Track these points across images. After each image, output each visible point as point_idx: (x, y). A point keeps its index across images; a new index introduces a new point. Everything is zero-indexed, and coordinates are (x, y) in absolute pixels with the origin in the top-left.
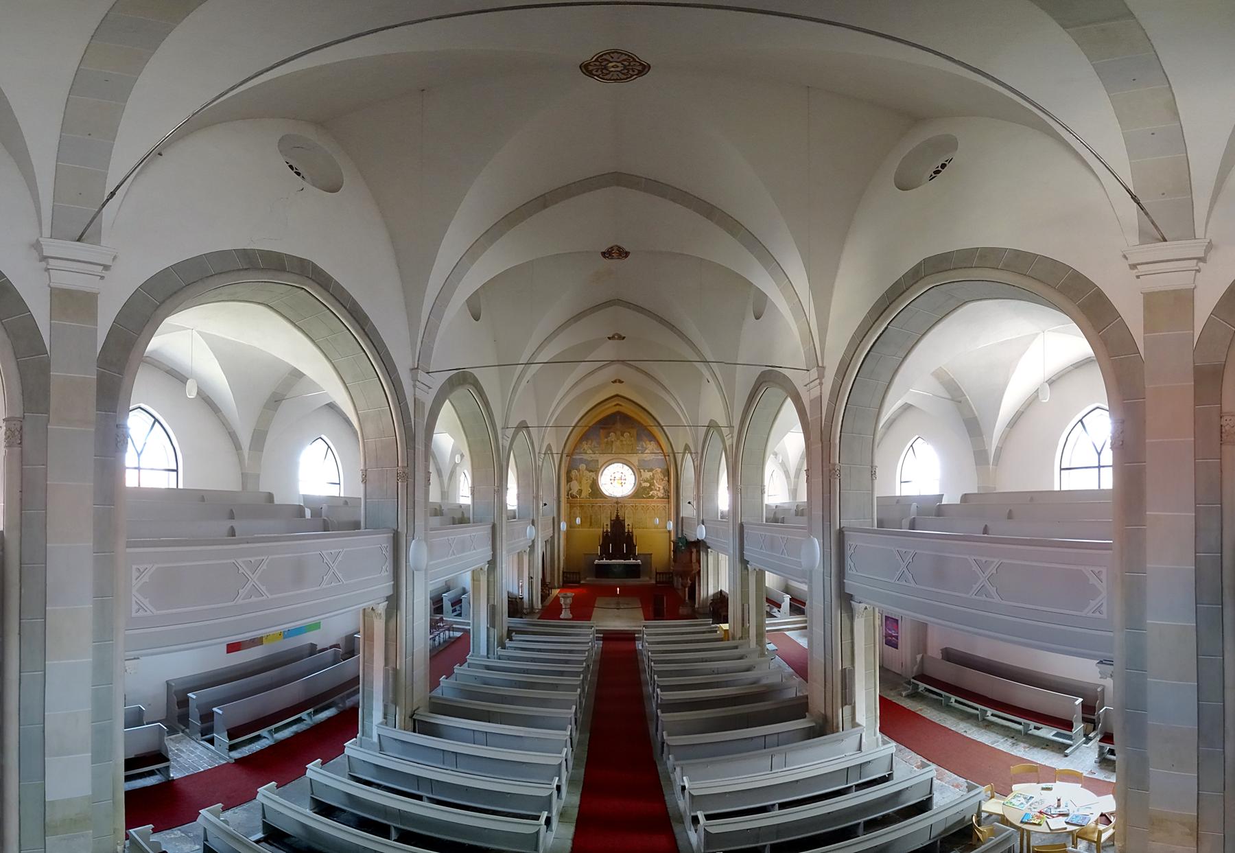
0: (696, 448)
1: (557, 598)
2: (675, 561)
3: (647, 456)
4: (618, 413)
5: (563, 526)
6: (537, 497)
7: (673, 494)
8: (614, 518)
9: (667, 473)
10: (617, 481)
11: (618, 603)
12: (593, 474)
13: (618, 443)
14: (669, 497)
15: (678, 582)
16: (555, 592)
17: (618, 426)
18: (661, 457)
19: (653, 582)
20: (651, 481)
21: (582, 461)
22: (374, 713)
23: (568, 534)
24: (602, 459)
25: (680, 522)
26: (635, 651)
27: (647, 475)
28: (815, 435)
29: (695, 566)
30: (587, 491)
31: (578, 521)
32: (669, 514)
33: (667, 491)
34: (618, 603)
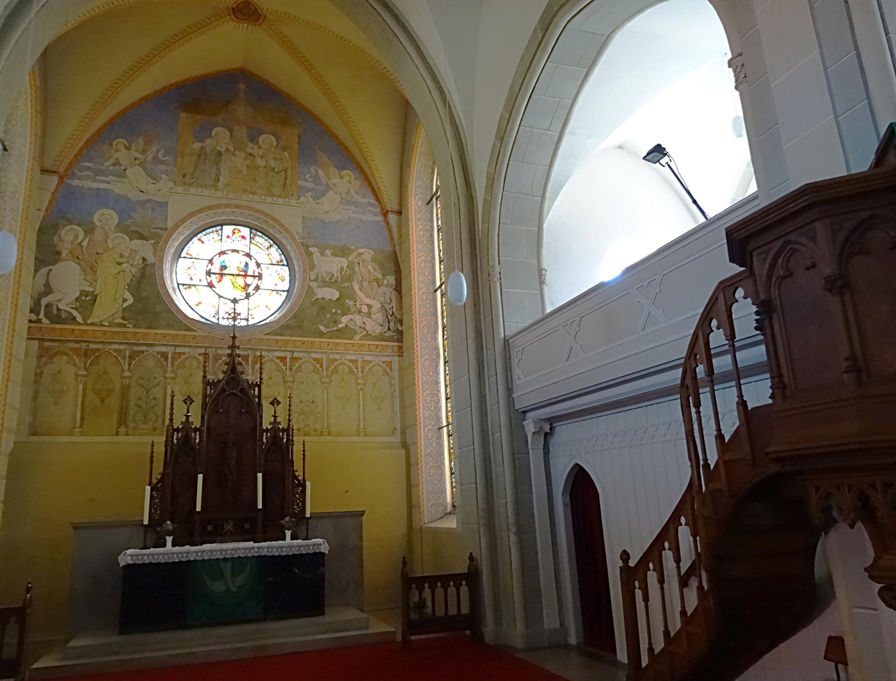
8: (217, 373)
12: (144, 249)
13: (239, 160)
17: (241, 110)
18: (372, 216)
20: (342, 283)
21: (103, 199)
22: (837, 590)
24: (182, 202)
27: (332, 265)
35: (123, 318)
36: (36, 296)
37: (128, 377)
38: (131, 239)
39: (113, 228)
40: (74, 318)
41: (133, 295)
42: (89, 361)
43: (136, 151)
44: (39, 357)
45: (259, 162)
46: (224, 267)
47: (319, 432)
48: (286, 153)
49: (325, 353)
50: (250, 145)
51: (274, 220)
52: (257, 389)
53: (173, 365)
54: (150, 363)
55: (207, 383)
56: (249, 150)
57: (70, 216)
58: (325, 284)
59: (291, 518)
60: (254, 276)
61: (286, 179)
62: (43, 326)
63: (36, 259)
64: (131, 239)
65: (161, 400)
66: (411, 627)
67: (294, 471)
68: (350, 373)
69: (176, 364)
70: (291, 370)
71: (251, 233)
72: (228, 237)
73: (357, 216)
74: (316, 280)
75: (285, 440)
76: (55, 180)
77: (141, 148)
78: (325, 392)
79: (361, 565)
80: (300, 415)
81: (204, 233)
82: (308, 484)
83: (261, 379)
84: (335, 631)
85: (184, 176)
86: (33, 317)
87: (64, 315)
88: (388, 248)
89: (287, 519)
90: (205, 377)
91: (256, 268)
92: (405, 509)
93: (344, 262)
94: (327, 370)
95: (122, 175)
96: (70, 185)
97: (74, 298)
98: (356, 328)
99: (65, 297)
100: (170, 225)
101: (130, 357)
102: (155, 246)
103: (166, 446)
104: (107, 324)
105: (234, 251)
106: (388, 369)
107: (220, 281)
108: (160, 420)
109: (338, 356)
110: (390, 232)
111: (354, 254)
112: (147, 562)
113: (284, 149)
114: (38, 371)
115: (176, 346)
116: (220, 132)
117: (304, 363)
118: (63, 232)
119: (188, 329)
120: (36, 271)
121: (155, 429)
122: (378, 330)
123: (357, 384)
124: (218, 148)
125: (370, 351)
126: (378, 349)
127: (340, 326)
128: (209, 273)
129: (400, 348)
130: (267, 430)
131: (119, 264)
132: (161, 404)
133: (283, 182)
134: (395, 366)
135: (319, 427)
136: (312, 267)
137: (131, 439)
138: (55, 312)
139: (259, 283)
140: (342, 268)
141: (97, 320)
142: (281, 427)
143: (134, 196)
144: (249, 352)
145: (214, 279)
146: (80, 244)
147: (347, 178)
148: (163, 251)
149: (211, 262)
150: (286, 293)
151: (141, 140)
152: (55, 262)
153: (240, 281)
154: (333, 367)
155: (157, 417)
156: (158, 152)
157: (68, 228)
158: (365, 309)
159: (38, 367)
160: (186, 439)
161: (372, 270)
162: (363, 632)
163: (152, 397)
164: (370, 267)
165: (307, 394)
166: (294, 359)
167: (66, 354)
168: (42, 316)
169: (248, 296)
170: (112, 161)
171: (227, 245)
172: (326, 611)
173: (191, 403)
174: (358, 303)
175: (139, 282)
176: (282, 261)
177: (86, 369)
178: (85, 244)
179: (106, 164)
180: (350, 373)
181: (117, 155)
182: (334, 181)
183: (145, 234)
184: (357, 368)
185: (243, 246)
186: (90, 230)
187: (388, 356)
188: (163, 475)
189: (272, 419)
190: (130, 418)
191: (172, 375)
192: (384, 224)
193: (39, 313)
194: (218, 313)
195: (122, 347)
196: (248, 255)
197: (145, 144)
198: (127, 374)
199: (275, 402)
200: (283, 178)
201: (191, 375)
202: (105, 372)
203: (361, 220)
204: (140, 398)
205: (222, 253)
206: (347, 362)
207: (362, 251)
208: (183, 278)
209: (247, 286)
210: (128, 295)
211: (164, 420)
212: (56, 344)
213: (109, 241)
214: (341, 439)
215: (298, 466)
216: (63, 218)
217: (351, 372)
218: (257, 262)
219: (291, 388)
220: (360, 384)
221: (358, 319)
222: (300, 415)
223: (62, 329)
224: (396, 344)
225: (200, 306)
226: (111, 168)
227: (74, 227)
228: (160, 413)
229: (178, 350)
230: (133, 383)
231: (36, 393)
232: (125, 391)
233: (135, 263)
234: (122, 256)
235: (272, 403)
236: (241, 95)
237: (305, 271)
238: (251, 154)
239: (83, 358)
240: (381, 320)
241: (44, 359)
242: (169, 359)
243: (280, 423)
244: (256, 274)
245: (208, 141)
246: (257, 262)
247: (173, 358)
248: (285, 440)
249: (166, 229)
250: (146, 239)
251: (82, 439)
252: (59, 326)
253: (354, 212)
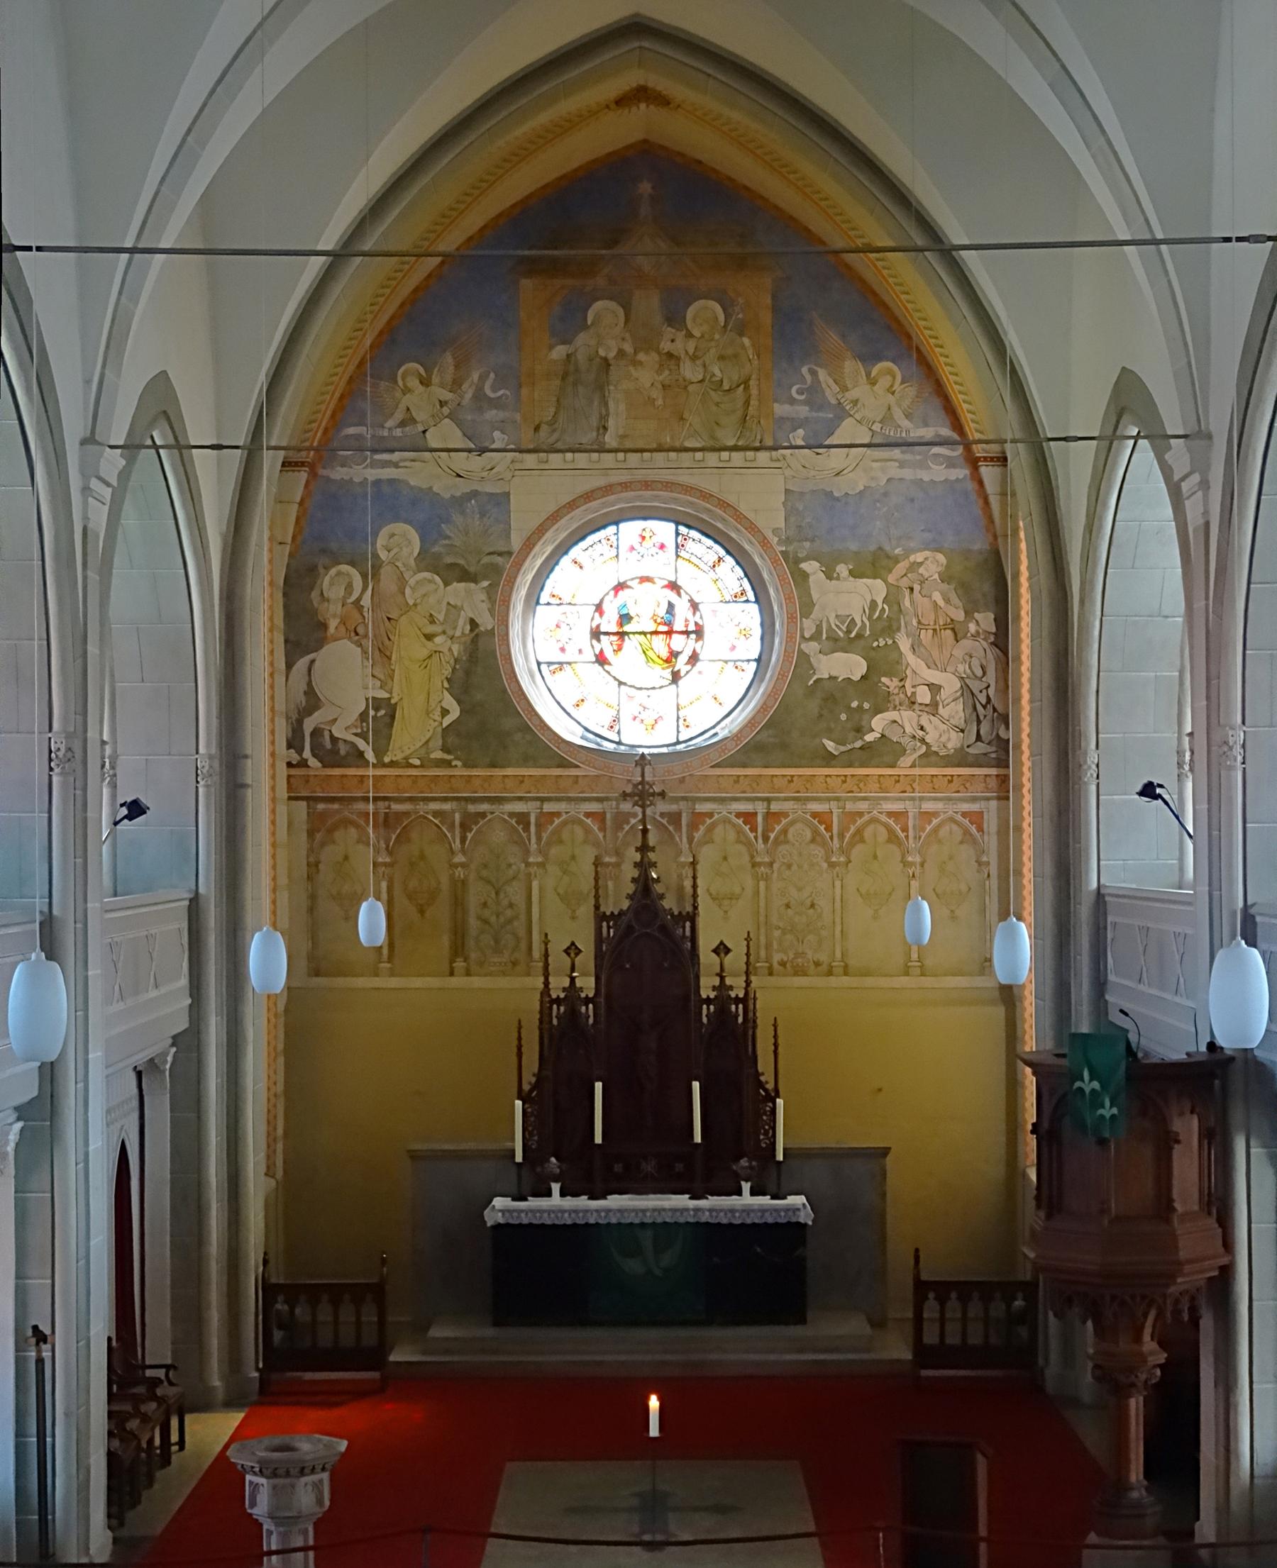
0: (1195, 390)
1: (224, 1478)
2: (1051, 1196)
3: (850, 470)
4: (646, 157)
5: (268, 961)
6: (72, 759)
7: (1034, 727)
8: (618, 899)
9: (991, 584)
10: (637, 639)
11: (653, 1506)
12: (470, 600)
13: (646, 376)
14: (1001, 754)
15: (1070, 1354)
16: (211, 1431)
17: (646, 250)
18: (943, 470)
19: (898, 1350)
20: (874, 638)
21: (392, 502)
23: (300, 1019)
24: (534, 487)
25: (1080, 926)
26: (497, 1227)
27: (848, 598)
28: (1047, 1110)
29: (1192, 1240)
30: (427, 711)
31: (371, 922)
32: (1007, 873)
33: (989, 715)
34: (653, 1506)
35: (445, 749)
36: (295, 716)
37: (463, 865)
38: (446, 584)
39: (412, 562)
40: (361, 754)
41: (459, 702)
42: (394, 837)
43: (442, 386)
44: (311, 833)
45: (690, 371)
46: (625, 618)
47: (825, 967)
48: (746, 341)
49: (837, 799)
50: (669, 332)
51: (724, 505)
52: (688, 924)
53: (539, 838)
54: (498, 836)
55: (600, 917)
56: (666, 346)
57: (334, 546)
58: (837, 644)
59: (750, 1161)
60: (687, 633)
61: (747, 403)
62: (312, 773)
63: (286, 641)
64: (446, 584)
65: (523, 906)
66: (924, 1355)
67: (758, 1074)
68: (889, 841)
69: (545, 836)
70: (766, 839)
71: (677, 534)
72: (632, 548)
73: (907, 474)
74: (816, 637)
75: (740, 1020)
76: (303, 476)
77: (449, 378)
78: (838, 883)
79: (883, 1239)
80: (784, 932)
81: (583, 545)
82: (780, 1102)
83: (695, 908)
84: (815, 1351)
85: (537, 429)
86: (295, 758)
87: (343, 750)
88: (980, 544)
89: (744, 1162)
90: (597, 907)
91: (689, 615)
92: (1002, 1126)
93: (877, 589)
94: (841, 836)
95: (419, 447)
96: (328, 479)
97: (356, 715)
98: (905, 741)
99: (342, 715)
100: (516, 543)
101: (462, 825)
102: (491, 591)
103: (540, 1029)
104: (417, 762)
105: (645, 579)
106: (973, 829)
107: (620, 648)
108: (523, 945)
109: (863, 806)
110: (986, 501)
111: (901, 567)
112: (525, 1221)
113: (741, 330)
114: (311, 859)
115: (542, 800)
116: (604, 310)
117: (792, 823)
118: (327, 580)
119: (564, 764)
120: (289, 666)
121: (514, 964)
122: (954, 741)
123: (906, 864)
124: (602, 353)
125: (934, 790)
126: (955, 786)
127: (869, 738)
128: (596, 634)
129: (1003, 780)
130: (708, 1001)
131: (429, 637)
132: (523, 917)
133: (739, 413)
134: (991, 823)
135: (823, 957)
136: (807, 606)
137: (476, 982)
138: (328, 745)
139: (698, 646)
140: (873, 604)
141: (399, 757)
142: (733, 994)
143: (445, 487)
144: (683, 805)
145: (606, 644)
146: (357, 603)
147: (884, 382)
148: (506, 603)
149: (599, 608)
150: (754, 665)
151: (448, 359)
152: (319, 644)
153: (659, 644)
154: (853, 829)
155: (518, 939)
156: (483, 378)
157: (333, 571)
158: (924, 696)
159: (311, 850)
160: (573, 1014)
161: (941, 603)
162: (865, 1356)
163: (505, 902)
164: (937, 596)
165: (800, 889)
166: (771, 816)
167: (353, 823)
168: (307, 753)
169: (676, 677)
170: (399, 415)
171: (628, 569)
172: (810, 1315)
173: (577, 954)
174: (908, 684)
175: (468, 673)
176: (743, 593)
177: (390, 852)
178: (366, 601)
179: (389, 424)
180: (889, 841)
181: (406, 400)
182: (853, 394)
183: (472, 569)
184: (905, 830)
185: (662, 566)
186: (372, 572)
187: (974, 800)
188: (539, 1076)
189: (717, 981)
190: (471, 943)
191: (540, 859)
192: (971, 486)
193: (303, 750)
194: (616, 720)
195: (447, 807)
196: (674, 586)
197: (457, 367)
198: (459, 858)
199: (722, 949)
200: (740, 404)
201: (573, 857)
202: (422, 857)
203: (919, 483)
204: (485, 905)
205: (620, 587)
206: (884, 818)
207: (919, 557)
208: (547, 652)
209: (674, 655)
210: (450, 702)
211: (530, 949)
212: (336, 806)
213: (408, 591)
214: (869, 981)
215: (764, 1064)
216: (323, 551)
217: (892, 838)
218: (691, 601)
219: (767, 879)
220: (911, 864)
221: (908, 719)
222: (784, 932)
223: (343, 776)
224: (993, 771)
225: (583, 707)
226: (398, 432)
227: (345, 568)
228: (522, 933)
229: (548, 807)
230: (472, 877)
231: (313, 897)
232: (459, 887)
233: (458, 633)
234: (432, 620)
235: (716, 951)
236: (645, 210)
237: (791, 618)
238: (670, 355)
239: (382, 830)
240: (959, 718)
241: (318, 836)
242: (533, 829)
243: (731, 988)
244: (692, 627)
245: (582, 339)
246: (691, 601)
247: (538, 825)
248: (740, 1020)
249: (510, 553)
250: (474, 579)
251: (394, 982)
252: (337, 772)
253: (902, 465)
